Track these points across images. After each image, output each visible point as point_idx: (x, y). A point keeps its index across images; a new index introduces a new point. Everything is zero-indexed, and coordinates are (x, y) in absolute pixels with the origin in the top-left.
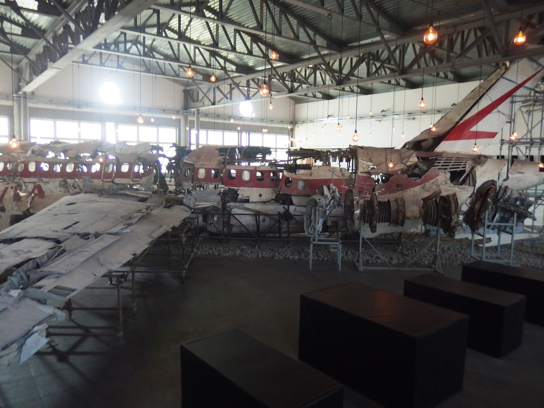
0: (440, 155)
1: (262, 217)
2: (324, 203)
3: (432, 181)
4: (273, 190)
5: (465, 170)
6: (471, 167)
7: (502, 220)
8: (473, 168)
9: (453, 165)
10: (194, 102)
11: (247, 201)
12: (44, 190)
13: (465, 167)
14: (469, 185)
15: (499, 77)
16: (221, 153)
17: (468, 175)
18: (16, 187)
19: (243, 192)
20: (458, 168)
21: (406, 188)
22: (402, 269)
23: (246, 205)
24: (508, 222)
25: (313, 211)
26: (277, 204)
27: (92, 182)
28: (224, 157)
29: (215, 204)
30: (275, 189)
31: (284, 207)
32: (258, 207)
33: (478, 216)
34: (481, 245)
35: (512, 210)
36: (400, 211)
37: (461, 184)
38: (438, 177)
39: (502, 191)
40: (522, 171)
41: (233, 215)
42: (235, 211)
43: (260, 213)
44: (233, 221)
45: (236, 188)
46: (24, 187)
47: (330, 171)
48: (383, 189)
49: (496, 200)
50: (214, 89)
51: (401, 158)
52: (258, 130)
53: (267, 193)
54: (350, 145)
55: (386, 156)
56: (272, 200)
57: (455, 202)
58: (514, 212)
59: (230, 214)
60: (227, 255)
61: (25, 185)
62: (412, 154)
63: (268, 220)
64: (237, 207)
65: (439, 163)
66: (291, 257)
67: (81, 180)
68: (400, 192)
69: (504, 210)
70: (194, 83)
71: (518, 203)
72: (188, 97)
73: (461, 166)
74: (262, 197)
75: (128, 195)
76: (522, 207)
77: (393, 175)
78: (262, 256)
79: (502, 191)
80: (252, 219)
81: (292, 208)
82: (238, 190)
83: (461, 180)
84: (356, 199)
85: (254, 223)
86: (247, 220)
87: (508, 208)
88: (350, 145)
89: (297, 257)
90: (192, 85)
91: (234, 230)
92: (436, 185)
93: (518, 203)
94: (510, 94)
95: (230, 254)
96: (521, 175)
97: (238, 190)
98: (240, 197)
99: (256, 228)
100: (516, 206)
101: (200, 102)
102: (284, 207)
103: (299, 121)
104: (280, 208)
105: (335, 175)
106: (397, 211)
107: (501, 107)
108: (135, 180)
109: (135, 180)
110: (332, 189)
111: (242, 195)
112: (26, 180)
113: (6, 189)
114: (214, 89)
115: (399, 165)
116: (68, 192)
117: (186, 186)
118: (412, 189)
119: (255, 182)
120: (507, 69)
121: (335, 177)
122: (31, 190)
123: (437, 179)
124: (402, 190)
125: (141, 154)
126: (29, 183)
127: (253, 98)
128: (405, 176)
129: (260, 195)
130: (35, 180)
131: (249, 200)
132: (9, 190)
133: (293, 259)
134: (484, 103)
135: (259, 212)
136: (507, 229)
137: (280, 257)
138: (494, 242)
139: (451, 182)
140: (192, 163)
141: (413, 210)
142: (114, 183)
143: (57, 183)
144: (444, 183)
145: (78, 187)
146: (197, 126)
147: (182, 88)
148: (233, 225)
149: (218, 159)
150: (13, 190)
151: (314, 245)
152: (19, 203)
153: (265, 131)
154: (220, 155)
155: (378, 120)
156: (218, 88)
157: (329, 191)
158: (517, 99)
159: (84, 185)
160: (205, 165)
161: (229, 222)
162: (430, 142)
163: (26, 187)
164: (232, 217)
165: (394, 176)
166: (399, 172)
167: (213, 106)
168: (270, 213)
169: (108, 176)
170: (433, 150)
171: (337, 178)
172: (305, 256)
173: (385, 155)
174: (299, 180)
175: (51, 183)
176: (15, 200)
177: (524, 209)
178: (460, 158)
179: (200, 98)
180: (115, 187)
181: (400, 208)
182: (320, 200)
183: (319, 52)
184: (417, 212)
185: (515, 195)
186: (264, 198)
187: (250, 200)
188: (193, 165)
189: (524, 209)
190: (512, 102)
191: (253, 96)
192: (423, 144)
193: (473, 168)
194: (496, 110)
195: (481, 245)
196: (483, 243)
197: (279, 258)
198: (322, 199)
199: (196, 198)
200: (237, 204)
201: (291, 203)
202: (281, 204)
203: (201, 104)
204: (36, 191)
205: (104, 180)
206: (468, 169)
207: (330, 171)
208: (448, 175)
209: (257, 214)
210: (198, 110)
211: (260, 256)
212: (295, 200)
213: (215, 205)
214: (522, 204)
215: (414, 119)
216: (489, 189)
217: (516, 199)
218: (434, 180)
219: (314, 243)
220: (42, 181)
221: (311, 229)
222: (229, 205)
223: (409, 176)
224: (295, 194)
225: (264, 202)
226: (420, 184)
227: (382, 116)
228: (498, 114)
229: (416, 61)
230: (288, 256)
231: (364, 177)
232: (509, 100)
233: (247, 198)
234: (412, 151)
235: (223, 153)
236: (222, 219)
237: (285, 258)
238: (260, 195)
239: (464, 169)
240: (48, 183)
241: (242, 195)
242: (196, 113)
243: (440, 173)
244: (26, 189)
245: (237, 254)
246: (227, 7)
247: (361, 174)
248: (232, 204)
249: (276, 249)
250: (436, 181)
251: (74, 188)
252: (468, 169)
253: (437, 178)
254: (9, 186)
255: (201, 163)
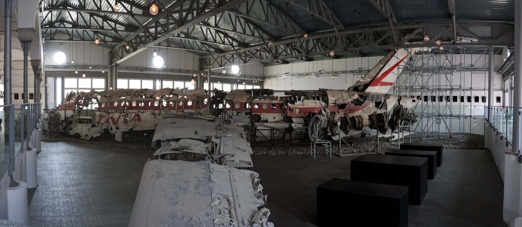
0: (368, 94)
1: (275, 131)
2: (323, 119)
3: (367, 107)
4: (282, 115)
5: (381, 101)
6: (384, 100)
7: (405, 124)
8: (385, 100)
9: (376, 99)
10: (207, 65)
11: (266, 121)
12: (141, 117)
13: (381, 100)
14: (384, 109)
15: (392, 56)
16: (247, 94)
17: (383, 104)
18: (125, 115)
19: (264, 116)
20: (378, 100)
21: (355, 111)
22: (361, 154)
23: (266, 124)
24: (407, 125)
25: (314, 124)
26: (284, 123)
27: (170, 112)
28: (250, 96)
29: (247, 124)
30: (283, 114)
31: (289, 124)
32: (272, 125)
33: (396, 122)
34: (390, 140)
35: (409, 119)
36: (361, 122)
37: (380, 109)
38: (369, 105)
39: (405, 110)
40: (406, 102)
41: (258, 130)
42: (259, 128)
43: (274, 129)
44: (258, 134)
45: (259, 114)
46: (129, 115)
47: (314, 102)
48: (343, 112)
49: (403, 115)
50: (221, 57)
51: (349, 95)
52: (241, 82)
53: (278, 116)
54: (320, 89)
55: (342, 94)
56: (282, 120)
57: (385, 116)
58: (410, 120)
59: (256, 129)
60: (259, 154)
61: (130, 114)
62: (355, 93)
63: (278, 132)
64: (260, 125)
65: (369, 98)
66: (298, 153)
67: (164, 111)
68: (352, 113)
69: (406, 119)
70: (210, 54)
71: (412, 116)
72: (203, 62)
73: (379, 99)
74: (276, 119)
75: (199, 118)
76: (413, 117)
77: (347, 104)
78: (280, 154)
79: (405, 110)
80: (269, 132)
81: (293, 125)
82: (260, 115)
83: (380, 106)
84: (338, 117)
85: (270, 135)
86: (266, 133)
87: (407, 118)
88: (320, 89)
89: (301, 153)
90: (208, 55)
91: (258, 139)
92: (369, 109)
93: (412, 116)
94: (397, 65)
95: (260, 153)
96: (405, 103)
97: (260, 115)
98: (262, 119)
99: (270, 138)
100: (411, 117)
101: (212, 65)
102: (289, 124)
103: (267, 77)
104: (286, 125)
105: (317, 105)
106: (359, 122)
107: (394, 70)
108: (196, 110)
109: (196, 110)
110: (327, 111)
111: (263, 118)
112: (130, 111)
113: (120, 116)
114: (221, 57)
115: (349, 99)
116: (156, 118)
117: (229, 113)
118: (357, 112)
119: (270, 110)
120: (395, 52)
121: (317, 106)
122: (133, 117)
123: (369, 106)
124: (353, 112)
125: (198, 95)
126: (132, 113)
127: (248, 62)
128: (354, 105)
129: (274, 118)
130: (136, 111)
131: (268, 121)
132: (121, 117)
133: (299, 154)
134: (387, 68)
135: (273, 128)
136: (407, 129)
137: (291, 154)
138: (396, 137)
139: (376, 107)
140: (231, 99)
141: (366, 121)
142: (183, 112)
143: (149, 113)
144: (372, 108)
145: (161, 115)
146: (209, 81)
147: (199, 57)
148: (257, 136)
149: (246, 97)
150: (124, 117)
151: (316, 144)
152: (127, 125)
153: (84, 75)
154: (248, 95)
155: (317, 76)
156: (224, 56)
157: (325, 113)
158: (400, 67)
159: (165, 114)
160: (239, 101)
161: (256, 134)
162: (362, 87)
163: (131, 115)
164: (257, 131)
165: (348, 105)
166: (350, 103)
167: (221, 68)
168: (280, 128)
169: (180, 108)
170: (364, 91)
171: (318, 106)
172: (305, 152)
173: (341, 94)
174: (296, 108)
175: (145, 113)
176: (124, 123)
177: (414, 119)
178: (378, 96)
179: (211, 63)
180: (184, 114)
181: (360, 120)
182: (320, 117)
183: (264, 41)
184: (368, 122)
185: (411, 112)
186: (276, 120)
187: (268, 121)
188: (232, 100)
189: (414, 119)
190: (399, 68)
191: (248, 61)
192: (359, 88)
193: (385, 100)
194: (392, 72)
195: (390, 140)
196: (391, 139)
197: (290, 154)
198: (322, 117)
199: (235, 121)
200: (260, 124)
201: (293, 122)
202: (287, 123)
203: (212, 66)
204: (136, 118)
205: (178, 110)
206: (383, 101)
207: (314, 102)
208: (374, 104)
209: (272, 129)
210: (210, 70)
211: (279, 154)
212: (294, 120)
213: (246, 124)
214: (413, 116)
215: (338, 76)
216: (400, 109)
217: (411, 114)
218: (368, 107)
219: (316, 143)
220: (140, 112)
221: (314, 135)
222: (256, 124)
223: (356, 105)
224: (295, 117)
225: (276, 122)
226: (361, 109)
227: (320, 74)
228: (393, 73)
229: (314, 47)
230: (296, 153)
231: (332, 106)
232: (396, 67)
233: (267, 120)
234: (355, 92)
235: (248, 94)
236: (249, 133)
237: (294, 154)
238: (274, 118)
239: (381, 101)
240: (144, 112)
241: (263, 118)
242: (209, 72)
243: (370, 103)
244: (131, 117)
245: (264, 153)
246: (132, 9)
247: (331, 104)
248: (257, 123)
249: (285, 150)
250: (369, 107)
251: (159, 116)
252: (383, 101)
253: (369, 105)
254: (122, 115)
255: (236, 99)
